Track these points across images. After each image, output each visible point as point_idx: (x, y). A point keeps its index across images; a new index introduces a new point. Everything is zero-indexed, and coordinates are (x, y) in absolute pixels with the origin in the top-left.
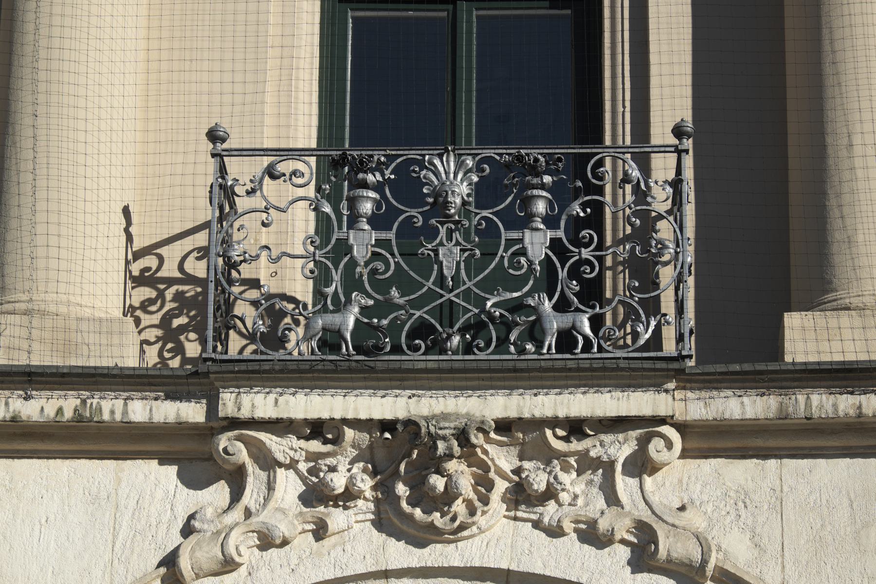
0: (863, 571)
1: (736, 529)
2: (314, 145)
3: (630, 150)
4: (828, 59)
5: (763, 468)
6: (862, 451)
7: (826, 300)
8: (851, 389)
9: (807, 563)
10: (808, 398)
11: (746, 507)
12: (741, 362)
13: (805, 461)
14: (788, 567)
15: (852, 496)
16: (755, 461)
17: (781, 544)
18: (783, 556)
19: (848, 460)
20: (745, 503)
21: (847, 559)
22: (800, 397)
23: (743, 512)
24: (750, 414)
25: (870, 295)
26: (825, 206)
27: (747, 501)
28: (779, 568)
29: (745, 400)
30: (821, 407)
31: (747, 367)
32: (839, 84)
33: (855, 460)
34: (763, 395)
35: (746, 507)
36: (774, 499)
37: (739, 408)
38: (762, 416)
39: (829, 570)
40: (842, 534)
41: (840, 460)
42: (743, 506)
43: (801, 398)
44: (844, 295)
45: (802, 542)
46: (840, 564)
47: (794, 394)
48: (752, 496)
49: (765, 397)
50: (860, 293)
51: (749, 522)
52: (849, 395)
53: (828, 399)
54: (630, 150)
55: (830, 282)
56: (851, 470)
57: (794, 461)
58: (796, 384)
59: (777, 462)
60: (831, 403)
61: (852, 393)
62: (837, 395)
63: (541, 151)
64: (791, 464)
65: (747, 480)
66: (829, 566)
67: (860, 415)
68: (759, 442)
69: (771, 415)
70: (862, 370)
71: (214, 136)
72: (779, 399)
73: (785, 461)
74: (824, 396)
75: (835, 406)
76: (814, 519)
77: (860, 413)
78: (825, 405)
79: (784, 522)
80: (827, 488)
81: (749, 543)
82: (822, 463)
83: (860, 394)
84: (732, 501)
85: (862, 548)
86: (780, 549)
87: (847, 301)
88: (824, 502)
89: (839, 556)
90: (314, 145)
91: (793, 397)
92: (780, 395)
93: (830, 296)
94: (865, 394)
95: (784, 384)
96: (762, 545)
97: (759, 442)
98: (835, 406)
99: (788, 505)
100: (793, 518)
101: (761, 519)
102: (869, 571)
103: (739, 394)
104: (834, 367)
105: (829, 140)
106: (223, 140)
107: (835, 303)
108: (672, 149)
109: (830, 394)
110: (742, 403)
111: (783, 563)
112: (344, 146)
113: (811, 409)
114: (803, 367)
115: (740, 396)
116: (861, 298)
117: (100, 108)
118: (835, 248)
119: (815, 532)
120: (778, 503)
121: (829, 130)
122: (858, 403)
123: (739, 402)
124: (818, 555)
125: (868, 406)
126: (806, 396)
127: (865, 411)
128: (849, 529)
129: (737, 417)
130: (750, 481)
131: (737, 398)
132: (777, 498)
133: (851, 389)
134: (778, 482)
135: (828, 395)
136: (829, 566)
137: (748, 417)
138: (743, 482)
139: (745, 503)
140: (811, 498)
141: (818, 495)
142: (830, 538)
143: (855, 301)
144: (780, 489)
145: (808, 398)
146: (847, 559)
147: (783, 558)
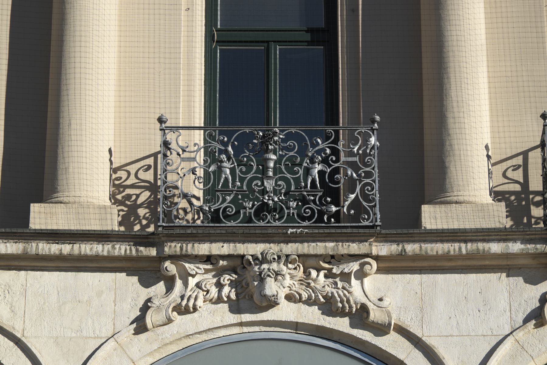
0: (61, 324)
1: (3, 303)
2: (202, 125)
3: (342, 128)
4: (64, 82)
5: (18, 275)
6: (65, 268)
7: (53, 197)
8: (57, 242)
9: (36, 320)
10: (37, 245)
11: (9, 293)
12: (5, 228)
13: (38, 272)
14: (26, 322)
15: (59, 289)
16: (14, 271)
17: (24, 311)
18: (24, 317)
19: (58, 273)
20: (8, 291)
21: (54, 319)
22: (33, 244)
23: (7, 295)
24: (9, 251)
25: (73, 196)
26: (57, 151)
27: (10, 290)
28: (22, 322)
29: (8, 244)
30: (43, 249)
31: (8, 230)
32: (68, 95)
33: (62, 273)
34: (16, 243)
35: (9, 293)
36: (22, 289)
37: (4, 248)
38: (15, 252)
39: (46, 324)
40: (53, 307)
41: (55, 272)
42: (7, 292)
43: (34, 245)
44: (62, 196)
45: (34, 310)
46: (51, 321)
47: (31, 243)
48: (12, 288)
49: (17, 244)
50: (68, 195)
51: (10, 300)
52: (56, 244)
53: (46, 246)
54: (342, 128)
55: (57, 188)
56: (59, 277)
57: (33, 272)
58: (31, 238)
59: (25, 272)
60: (48, 247)
61: (58, 243)
62: (51, 244)
63: (333, 128)
64: (31, 273)
65: (10, 280)
66: (46, 322)
67: (61, 254)
68: (16, 263)
69: (20, 252)
70: (61, 234)
71: (161, 120)
72: (24, 245)
73: (29, 272)
74: (45, 244)
75: (50, 249)
76: (41, 300)
77: (61, 253)
78: (45, 249)
79: (26, 301)
80: (48, 285)
81: (9, 310)
82: (46, 273)
83: (61, 244)
84: (2, 290)
85: (61, 314)
86: (23, 313)
87: (62, 199)
88: (46, 292)
89: (50, 317)
90: (202, 125)
91: (31, 244)
92: (25, 243)
93: (55, 195)
94: (64, 244)
95: (26, 238)
96: (15, 311)
97: (16, 263)
98: (50, 249)
99: (29, 293)
100: (31, 299)
101: (15, 299)
102: (64, 325)
103: (5, 242)
104: (48, 232)
105: (61, 121)
106: (165, 122)
107: (56, 199)
108: (370, 128)
109: (48, 243)
110: (6, 246)
111: (24, 320)
112: (216, 125)
113: (38, 250)
114: (34, 231)
115: (5, 243)
116: (68, 198)
117: (92, 112)
118: (60, 172)
119: (40, 306)
120: (24, 291)
121: (61, 116)
122: (60, 248)
123: (5, 245)
124: (41, 316)
125: (65, 250)
126: (36, 244)
127: (63, 252)
128: (56, 305)
129: (4, 253)
130: (11, 281)
131: (4, 244)
132: (24, 289)
133: (57, 242)
134: (25, 282)
135: (47, 244)
136: (46, 322)
137: (8, 253)
138: (8, 281)
139: (8, 291)
140: (40, 289)
141: (43, 288)
142: (47, 309)
143: (65, 199)
144: (25, 285)
145: (37, 245)
146: (54, 319)
147: (24, 318)
